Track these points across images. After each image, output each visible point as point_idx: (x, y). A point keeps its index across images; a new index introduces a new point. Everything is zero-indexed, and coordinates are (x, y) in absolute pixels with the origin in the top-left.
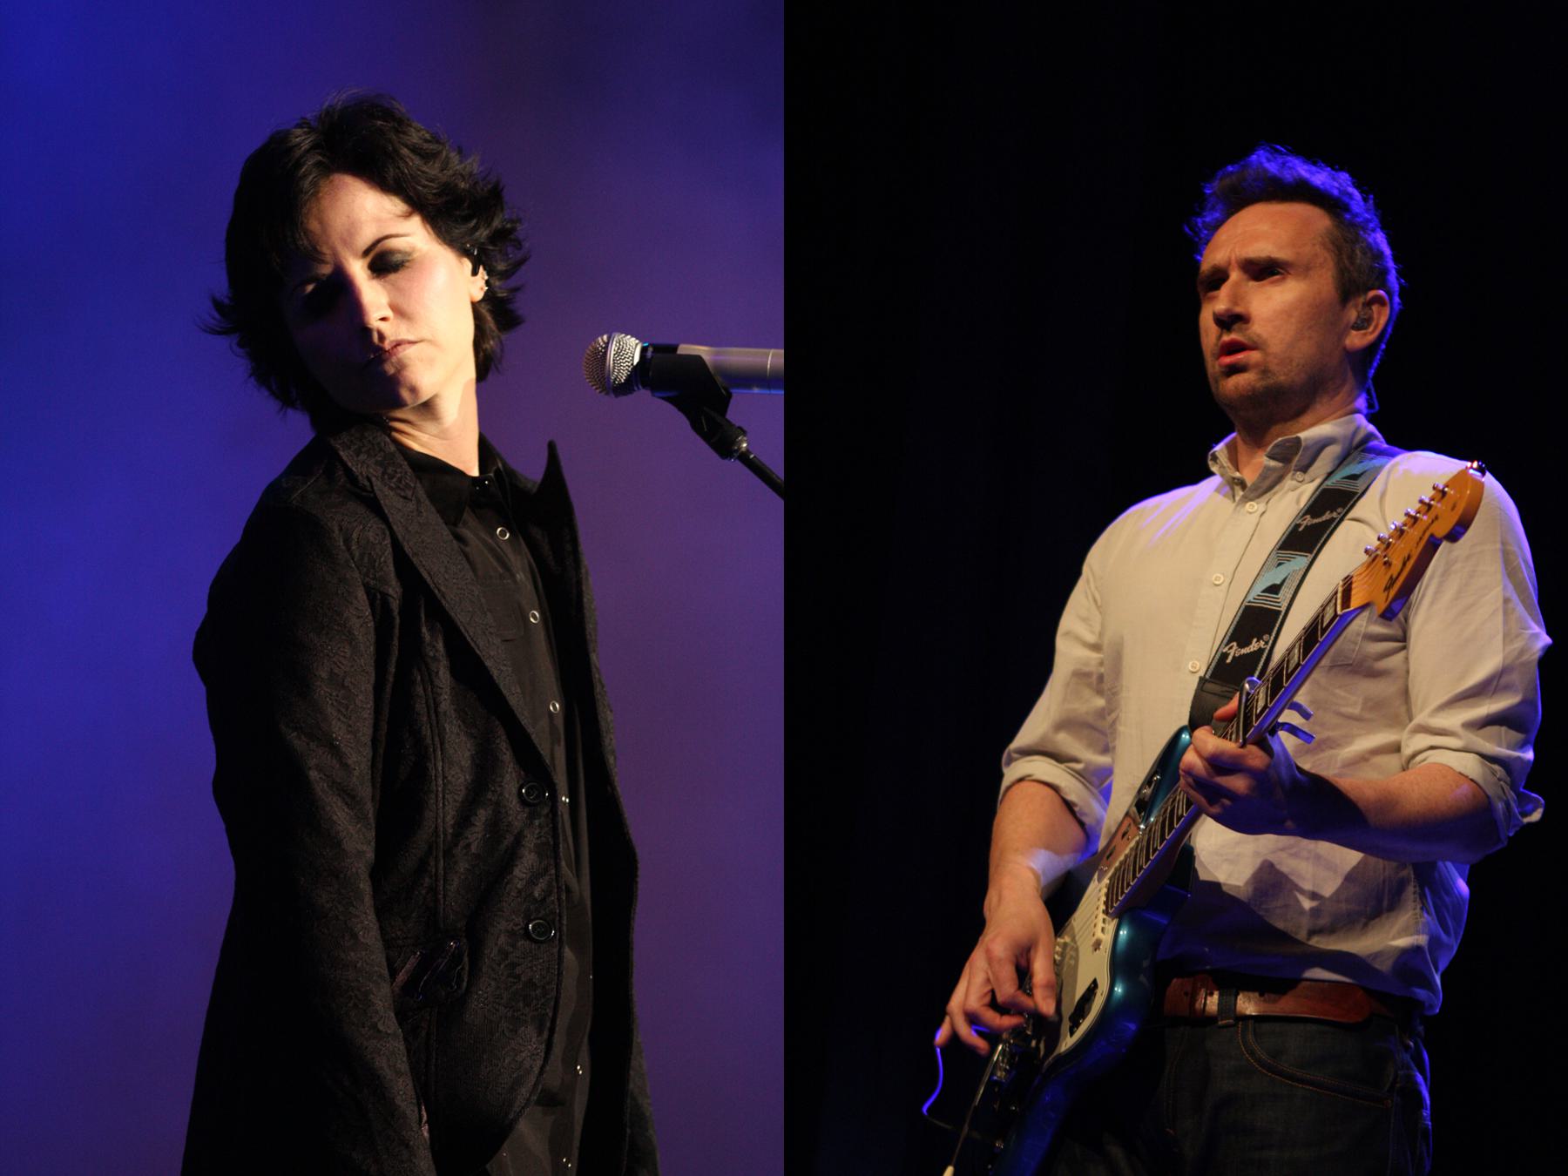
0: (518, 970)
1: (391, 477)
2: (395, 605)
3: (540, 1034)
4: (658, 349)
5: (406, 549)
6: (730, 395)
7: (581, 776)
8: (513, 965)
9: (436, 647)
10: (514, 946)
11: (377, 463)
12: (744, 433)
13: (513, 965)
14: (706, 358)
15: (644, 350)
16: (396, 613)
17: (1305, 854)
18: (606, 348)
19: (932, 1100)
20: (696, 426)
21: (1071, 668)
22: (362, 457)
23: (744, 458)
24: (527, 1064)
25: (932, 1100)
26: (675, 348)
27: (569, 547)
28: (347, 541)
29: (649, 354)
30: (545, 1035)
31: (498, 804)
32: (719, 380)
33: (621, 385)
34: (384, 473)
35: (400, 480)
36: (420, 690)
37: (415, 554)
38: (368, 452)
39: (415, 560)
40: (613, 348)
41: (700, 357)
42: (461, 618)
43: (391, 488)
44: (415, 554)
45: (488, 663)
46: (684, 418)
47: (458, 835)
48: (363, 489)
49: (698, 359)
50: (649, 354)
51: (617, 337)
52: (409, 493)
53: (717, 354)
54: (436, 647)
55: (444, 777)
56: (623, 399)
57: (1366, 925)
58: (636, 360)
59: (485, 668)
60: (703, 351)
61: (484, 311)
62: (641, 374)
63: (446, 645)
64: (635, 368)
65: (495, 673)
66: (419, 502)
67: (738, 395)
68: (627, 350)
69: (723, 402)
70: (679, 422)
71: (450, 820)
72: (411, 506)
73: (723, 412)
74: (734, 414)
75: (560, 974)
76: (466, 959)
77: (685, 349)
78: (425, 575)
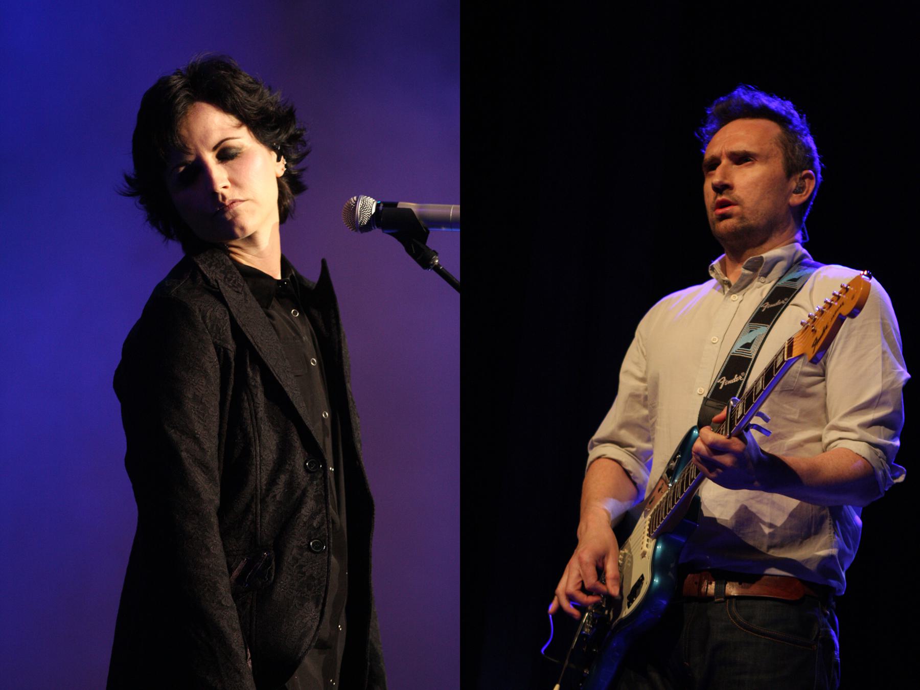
0: (304, 569)
1: (230, 280)
2: (232, 355)
3: (317, 606)
4: (386, 205)
5: (238, 322)
6: (428, 232)
7: (341, 455)
8: (301, 566)
9: (256, 380)
10: (301, 555)
11: (221, 272)
12: (437, 254)
13: (301, 566)
14: (414, 210)
15: (378, 205)
16: (232, 360)
17: (766, 501)
18: (356, 204)
19: (547, 645)
20: (408, 250)
21: (628, 392)
22: (213, 268)
23: (436, 269)
24: (309, 624)
25: (547, 645)
26: (396, 204)
27: (334, 321)
28: (204, 317)
29: (381, 208)
30: (320, 607)
31: (292, 472)
32: (422, 223)
33: (364, 226)
34: (225, 278)
35: (235, 282)
36: (246, 405)
37: (244, 325)
38: (216, 265)
39: (243, 329)
40: (360, 204)
41: (410, 210)
42: (270, 363)
43: (229, 286)
44: (244, 325)
45: (286, 389)
46: (401, 245)
47: (268, 490)
48: (213, 287)
49: (410, 211)
50: (381, 208)
51: (362, 198)
52: (240, 289)
53: (421, 208)
54: (256, 380)
55: (261, 456)
56: (366, 234)
57: (801, 543)
58: (373, 211)
59: (285, 392)
60: (412, 206)
61: (284, 182)
62: (376, 219)
63: (262, 379)
64: (373, 216)
65: (290, 395)
66: (246, 294)
67: (433, 232)
68: (368, 206)
69: (424, 236)
70: (398, 248)
71: (264, 481)
72: (241, 297)
73: (424, 242)
74: (431, 243)
75: (328, 571)
76: (273, 563)
77: (402, 205)
78: (249, 337)
